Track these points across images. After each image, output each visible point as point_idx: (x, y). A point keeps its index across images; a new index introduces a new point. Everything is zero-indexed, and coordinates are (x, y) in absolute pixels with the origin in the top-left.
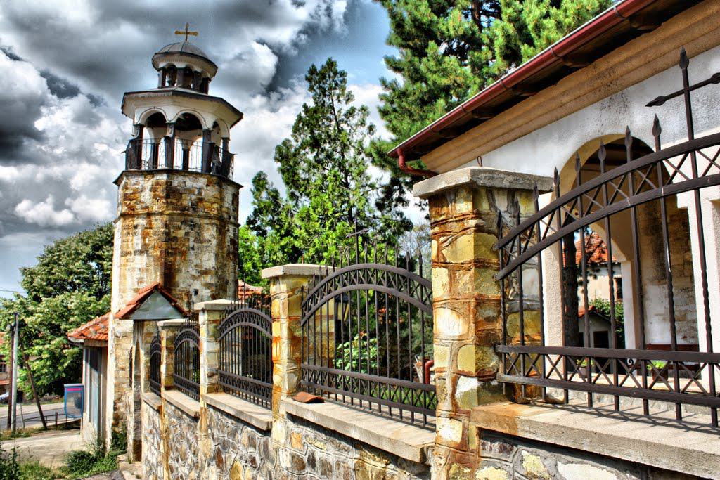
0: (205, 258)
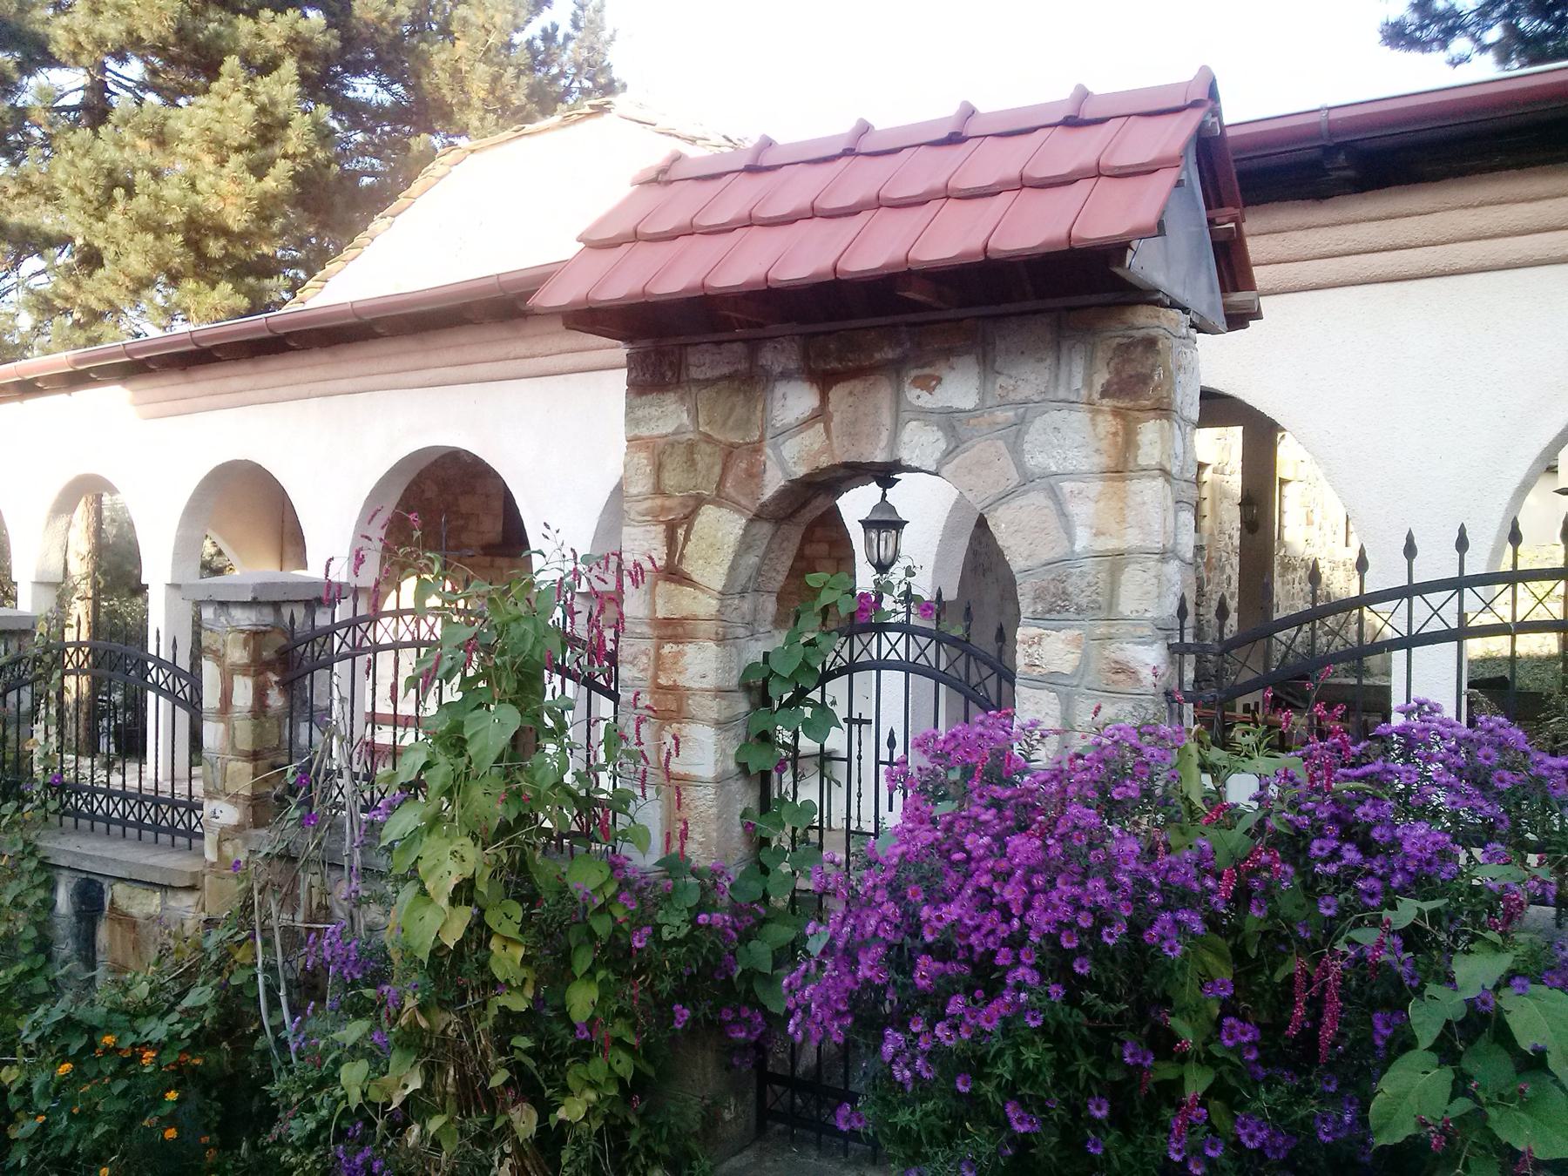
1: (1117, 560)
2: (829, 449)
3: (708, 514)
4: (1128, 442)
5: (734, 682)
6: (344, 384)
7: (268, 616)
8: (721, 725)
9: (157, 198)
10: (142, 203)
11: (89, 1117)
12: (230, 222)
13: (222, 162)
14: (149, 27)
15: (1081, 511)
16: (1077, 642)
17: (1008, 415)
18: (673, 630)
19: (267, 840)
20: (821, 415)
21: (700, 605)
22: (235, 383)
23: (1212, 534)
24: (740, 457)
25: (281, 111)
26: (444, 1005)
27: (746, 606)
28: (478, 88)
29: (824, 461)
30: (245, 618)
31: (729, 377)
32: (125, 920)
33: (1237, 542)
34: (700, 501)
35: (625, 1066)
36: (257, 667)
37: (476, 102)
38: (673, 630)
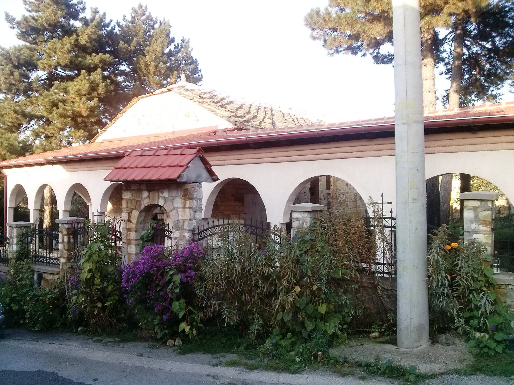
1: (184, 220)
2: (150, 202)
3: (134, 211)
4: (185, 204)
5: (139, 238)
6: (99, 168)
7: (70, 226)
8: (136, 245)
9: (64, 109)
10: (60, 110)
11: (37, 312)
12: (83, 114)
13: (81, 99)
14: (62, 62)
15: (180, 213)
16: (179, 233)
17: (171, 198)
18: (129, 230)
19: (69, 265)
20: (149, 196)
21: (133, 226)
22: (77, 166)
23: (333, 190)
24: (138, 202)
25: (97, 82)
26: (88, 288)
27: (142, 226)
28: (152, 69)
29: (149, 204)
30: (66, 226)
31: (136, 189)
32: (46, 280)
33: (309, 197)
34: (133, 209)
35: (117, 298)
36: (68, 235)
37: (152, 73)
38: (129, 230)
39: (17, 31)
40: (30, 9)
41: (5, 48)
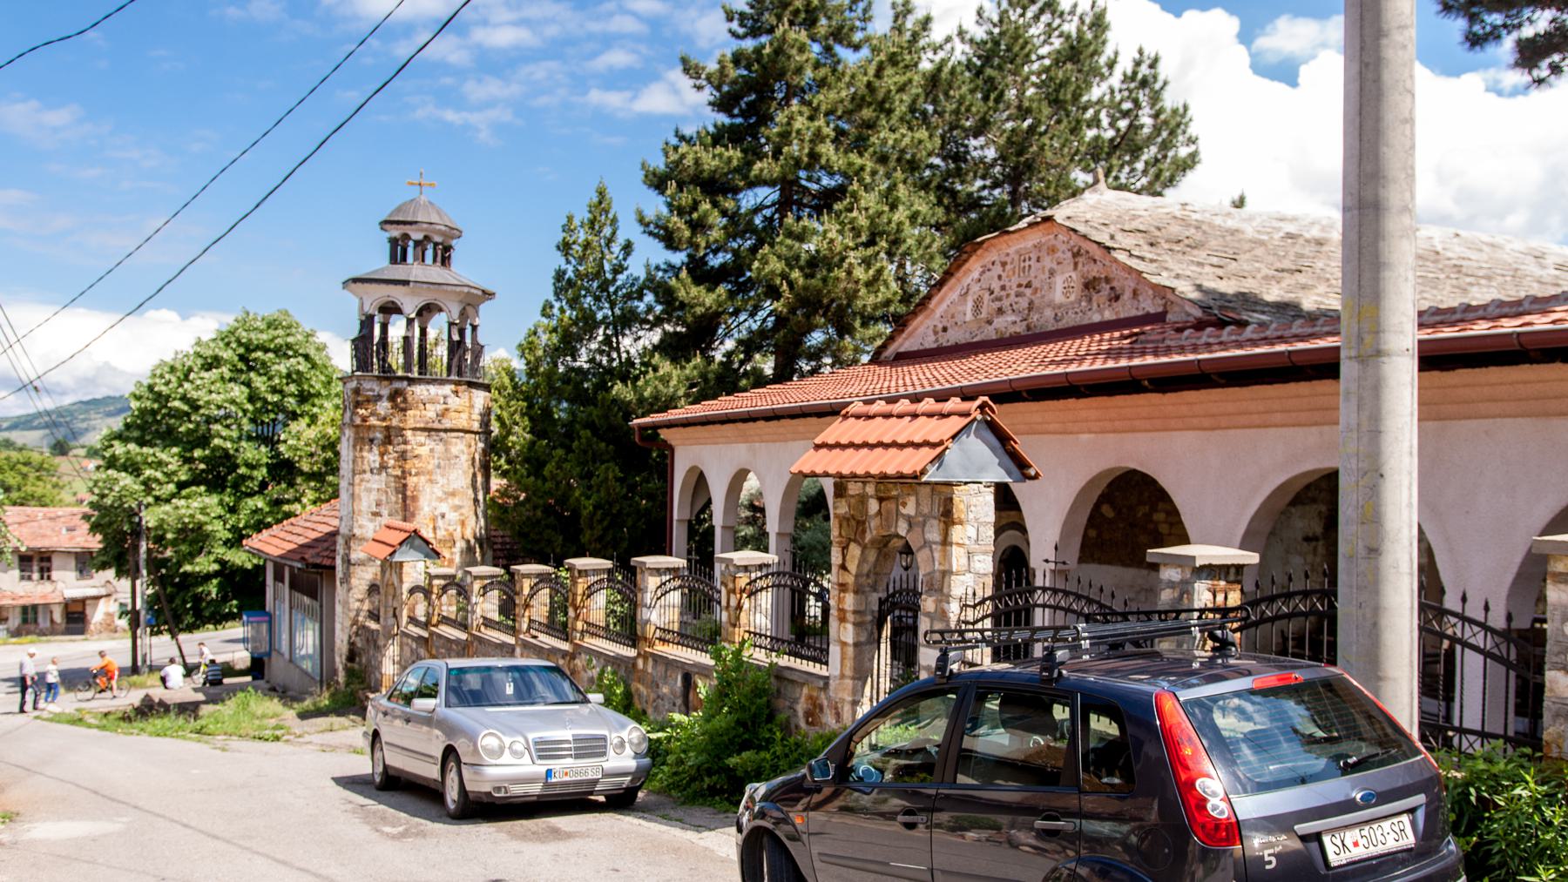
0: (453, 476)
3: (853, 546)
15: (937, 555)
21: (850, 579)
39: (708, 94)
40: (741, 31)
41: (1110, 35)
